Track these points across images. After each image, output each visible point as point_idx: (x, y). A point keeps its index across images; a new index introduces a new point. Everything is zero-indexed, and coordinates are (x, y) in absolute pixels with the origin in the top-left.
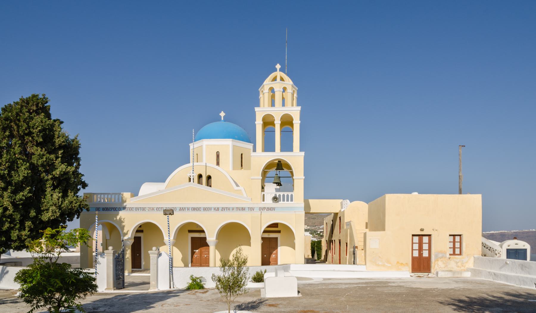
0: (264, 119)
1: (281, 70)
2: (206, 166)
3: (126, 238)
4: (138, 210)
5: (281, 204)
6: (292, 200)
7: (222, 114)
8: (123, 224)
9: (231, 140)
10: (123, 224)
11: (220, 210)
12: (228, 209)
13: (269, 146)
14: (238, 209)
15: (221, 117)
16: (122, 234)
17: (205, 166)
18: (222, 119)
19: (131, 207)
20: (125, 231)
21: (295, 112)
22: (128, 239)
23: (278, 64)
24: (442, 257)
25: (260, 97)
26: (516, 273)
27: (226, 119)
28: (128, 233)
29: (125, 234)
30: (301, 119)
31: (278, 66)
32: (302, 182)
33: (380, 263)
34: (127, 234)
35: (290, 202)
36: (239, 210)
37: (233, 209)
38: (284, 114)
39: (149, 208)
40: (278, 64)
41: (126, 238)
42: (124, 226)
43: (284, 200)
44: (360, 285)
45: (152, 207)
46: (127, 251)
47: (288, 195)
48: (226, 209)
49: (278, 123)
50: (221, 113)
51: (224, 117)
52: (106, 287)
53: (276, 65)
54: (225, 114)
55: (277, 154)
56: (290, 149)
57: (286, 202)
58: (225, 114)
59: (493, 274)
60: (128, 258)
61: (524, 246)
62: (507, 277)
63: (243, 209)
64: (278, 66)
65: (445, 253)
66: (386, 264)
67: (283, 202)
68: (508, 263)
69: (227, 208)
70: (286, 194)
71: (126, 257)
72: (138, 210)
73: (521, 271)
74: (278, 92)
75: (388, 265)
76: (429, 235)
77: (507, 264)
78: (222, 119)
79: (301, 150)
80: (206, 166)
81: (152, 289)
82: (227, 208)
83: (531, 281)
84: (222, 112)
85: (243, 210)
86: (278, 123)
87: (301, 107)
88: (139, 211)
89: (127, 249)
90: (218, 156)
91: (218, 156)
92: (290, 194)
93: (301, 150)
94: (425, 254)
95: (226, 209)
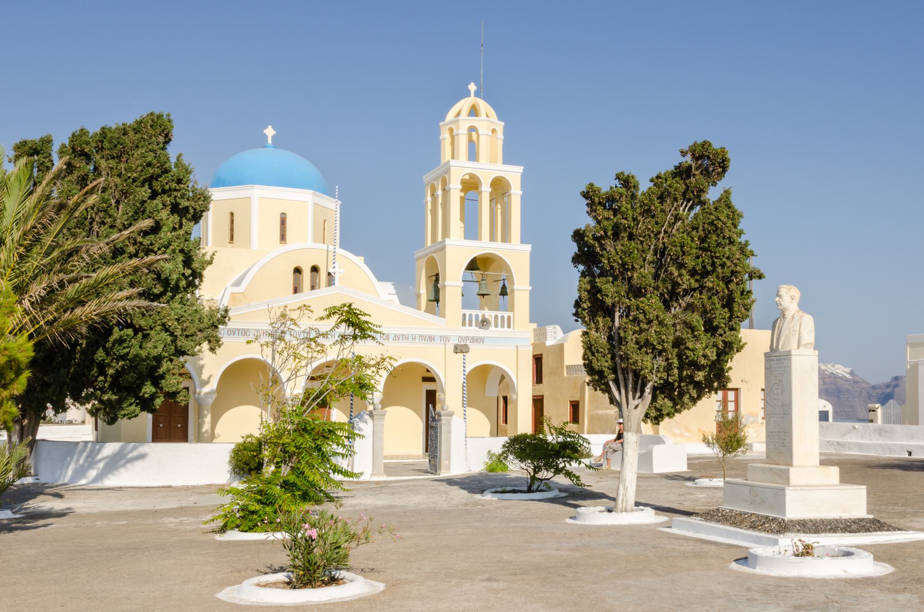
0: (463, 182)
1: (477, 94)
2: (328, 251)
3: (206, 389)
4: (234, 334)
5: (492, 331)
6: (509, 327)
7: (270, 132)
8: (202, 362)
9: (311, 191)
10: (202, 362)
11: (391, 340)
12: (405, 337)
13: (472, 232)
14: (423, 337)
15: (267, 137)
16: (197, 383)
17: (326, 252)
18: (270, 141)
19: (244, 330)
20: (205, 376)
21: (514, 174)
22: (210, 393)
23: (472, 84)
24: (753, 422)
25: (441, 137)
26: (871, 440)
27: (278, 142)
28: (211, 380)
29: (205, 383)
30: (523, 188)
31: (472, 87)
32: (527, 295)
33: (678, 432)
34: (207, 382)
35: (499, 328)
36: (425, 340)
37: (414, 338)
38: (494, 179)
39: (255, 330)
40: (472, 84)
41: (206, 389)
42: (202, 366)
43: (496, 326)
44: (694, 461)
45: (262, 330)
46: (206, 418)
47: (503, 317)
48: (237, 332)
49: (486, 189)
50: (267, 129)
51: (273, 137)
52: (371, 473)
53: (469, 84)
54: (265, 131)
55: (482, 247)
56: (506, 238)
57: (506, 329)
58: (274, 132)
59: (835, 443)
60: (207, 431)
61: (825, 407)
62: (860, 446)
63: (431, 338)
64: (472, 87)
65: (756, 416)
66: (685, 433)
67: (502, 329)
68: (857, 427)
69: (404, 337)
70: (500, 314)
71: (204, 430)
72: (234, 334)
73: (878, 437)
74: (485, 136)
75: (689, 435)
76: (736, 390)
77: (856, 429)
78: (270, 141)
79: (523, 241)
80: (328, 251)
81: (444, 473)
82: (404, 337)
83: (902, 448)
84: (270, 127)
85: (431, 341)
86: (486, 189)
87: (523, 167)
88: (235, 336)
89: (206, 412)
90: (283, 222)
91: (283, 222)
92: (506, 314)
93: (523, 241)
94: (730, 416)
95: (237, 332)
